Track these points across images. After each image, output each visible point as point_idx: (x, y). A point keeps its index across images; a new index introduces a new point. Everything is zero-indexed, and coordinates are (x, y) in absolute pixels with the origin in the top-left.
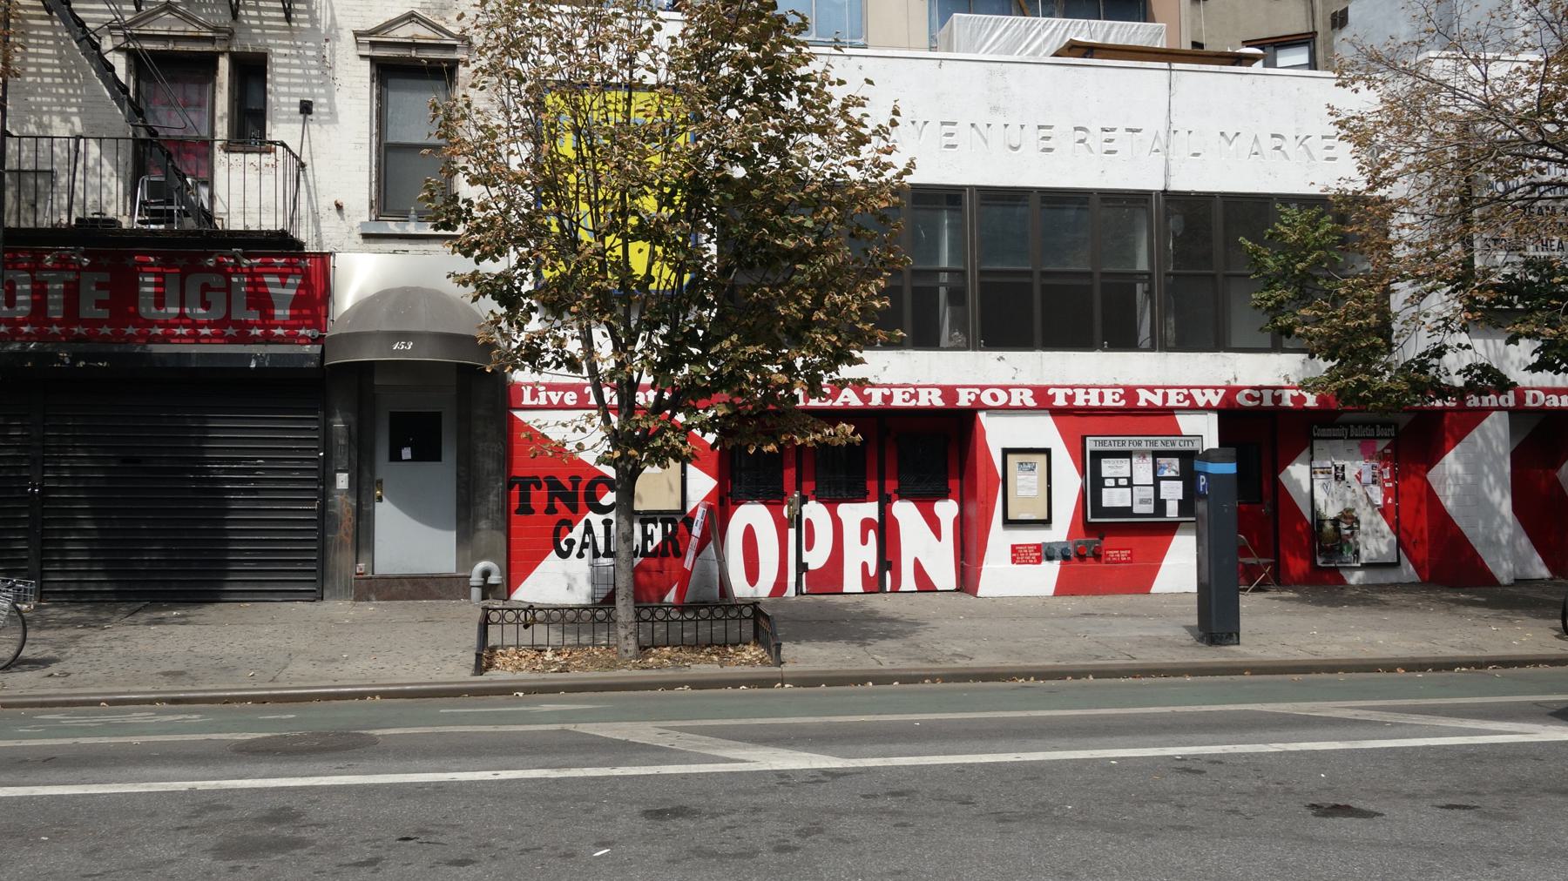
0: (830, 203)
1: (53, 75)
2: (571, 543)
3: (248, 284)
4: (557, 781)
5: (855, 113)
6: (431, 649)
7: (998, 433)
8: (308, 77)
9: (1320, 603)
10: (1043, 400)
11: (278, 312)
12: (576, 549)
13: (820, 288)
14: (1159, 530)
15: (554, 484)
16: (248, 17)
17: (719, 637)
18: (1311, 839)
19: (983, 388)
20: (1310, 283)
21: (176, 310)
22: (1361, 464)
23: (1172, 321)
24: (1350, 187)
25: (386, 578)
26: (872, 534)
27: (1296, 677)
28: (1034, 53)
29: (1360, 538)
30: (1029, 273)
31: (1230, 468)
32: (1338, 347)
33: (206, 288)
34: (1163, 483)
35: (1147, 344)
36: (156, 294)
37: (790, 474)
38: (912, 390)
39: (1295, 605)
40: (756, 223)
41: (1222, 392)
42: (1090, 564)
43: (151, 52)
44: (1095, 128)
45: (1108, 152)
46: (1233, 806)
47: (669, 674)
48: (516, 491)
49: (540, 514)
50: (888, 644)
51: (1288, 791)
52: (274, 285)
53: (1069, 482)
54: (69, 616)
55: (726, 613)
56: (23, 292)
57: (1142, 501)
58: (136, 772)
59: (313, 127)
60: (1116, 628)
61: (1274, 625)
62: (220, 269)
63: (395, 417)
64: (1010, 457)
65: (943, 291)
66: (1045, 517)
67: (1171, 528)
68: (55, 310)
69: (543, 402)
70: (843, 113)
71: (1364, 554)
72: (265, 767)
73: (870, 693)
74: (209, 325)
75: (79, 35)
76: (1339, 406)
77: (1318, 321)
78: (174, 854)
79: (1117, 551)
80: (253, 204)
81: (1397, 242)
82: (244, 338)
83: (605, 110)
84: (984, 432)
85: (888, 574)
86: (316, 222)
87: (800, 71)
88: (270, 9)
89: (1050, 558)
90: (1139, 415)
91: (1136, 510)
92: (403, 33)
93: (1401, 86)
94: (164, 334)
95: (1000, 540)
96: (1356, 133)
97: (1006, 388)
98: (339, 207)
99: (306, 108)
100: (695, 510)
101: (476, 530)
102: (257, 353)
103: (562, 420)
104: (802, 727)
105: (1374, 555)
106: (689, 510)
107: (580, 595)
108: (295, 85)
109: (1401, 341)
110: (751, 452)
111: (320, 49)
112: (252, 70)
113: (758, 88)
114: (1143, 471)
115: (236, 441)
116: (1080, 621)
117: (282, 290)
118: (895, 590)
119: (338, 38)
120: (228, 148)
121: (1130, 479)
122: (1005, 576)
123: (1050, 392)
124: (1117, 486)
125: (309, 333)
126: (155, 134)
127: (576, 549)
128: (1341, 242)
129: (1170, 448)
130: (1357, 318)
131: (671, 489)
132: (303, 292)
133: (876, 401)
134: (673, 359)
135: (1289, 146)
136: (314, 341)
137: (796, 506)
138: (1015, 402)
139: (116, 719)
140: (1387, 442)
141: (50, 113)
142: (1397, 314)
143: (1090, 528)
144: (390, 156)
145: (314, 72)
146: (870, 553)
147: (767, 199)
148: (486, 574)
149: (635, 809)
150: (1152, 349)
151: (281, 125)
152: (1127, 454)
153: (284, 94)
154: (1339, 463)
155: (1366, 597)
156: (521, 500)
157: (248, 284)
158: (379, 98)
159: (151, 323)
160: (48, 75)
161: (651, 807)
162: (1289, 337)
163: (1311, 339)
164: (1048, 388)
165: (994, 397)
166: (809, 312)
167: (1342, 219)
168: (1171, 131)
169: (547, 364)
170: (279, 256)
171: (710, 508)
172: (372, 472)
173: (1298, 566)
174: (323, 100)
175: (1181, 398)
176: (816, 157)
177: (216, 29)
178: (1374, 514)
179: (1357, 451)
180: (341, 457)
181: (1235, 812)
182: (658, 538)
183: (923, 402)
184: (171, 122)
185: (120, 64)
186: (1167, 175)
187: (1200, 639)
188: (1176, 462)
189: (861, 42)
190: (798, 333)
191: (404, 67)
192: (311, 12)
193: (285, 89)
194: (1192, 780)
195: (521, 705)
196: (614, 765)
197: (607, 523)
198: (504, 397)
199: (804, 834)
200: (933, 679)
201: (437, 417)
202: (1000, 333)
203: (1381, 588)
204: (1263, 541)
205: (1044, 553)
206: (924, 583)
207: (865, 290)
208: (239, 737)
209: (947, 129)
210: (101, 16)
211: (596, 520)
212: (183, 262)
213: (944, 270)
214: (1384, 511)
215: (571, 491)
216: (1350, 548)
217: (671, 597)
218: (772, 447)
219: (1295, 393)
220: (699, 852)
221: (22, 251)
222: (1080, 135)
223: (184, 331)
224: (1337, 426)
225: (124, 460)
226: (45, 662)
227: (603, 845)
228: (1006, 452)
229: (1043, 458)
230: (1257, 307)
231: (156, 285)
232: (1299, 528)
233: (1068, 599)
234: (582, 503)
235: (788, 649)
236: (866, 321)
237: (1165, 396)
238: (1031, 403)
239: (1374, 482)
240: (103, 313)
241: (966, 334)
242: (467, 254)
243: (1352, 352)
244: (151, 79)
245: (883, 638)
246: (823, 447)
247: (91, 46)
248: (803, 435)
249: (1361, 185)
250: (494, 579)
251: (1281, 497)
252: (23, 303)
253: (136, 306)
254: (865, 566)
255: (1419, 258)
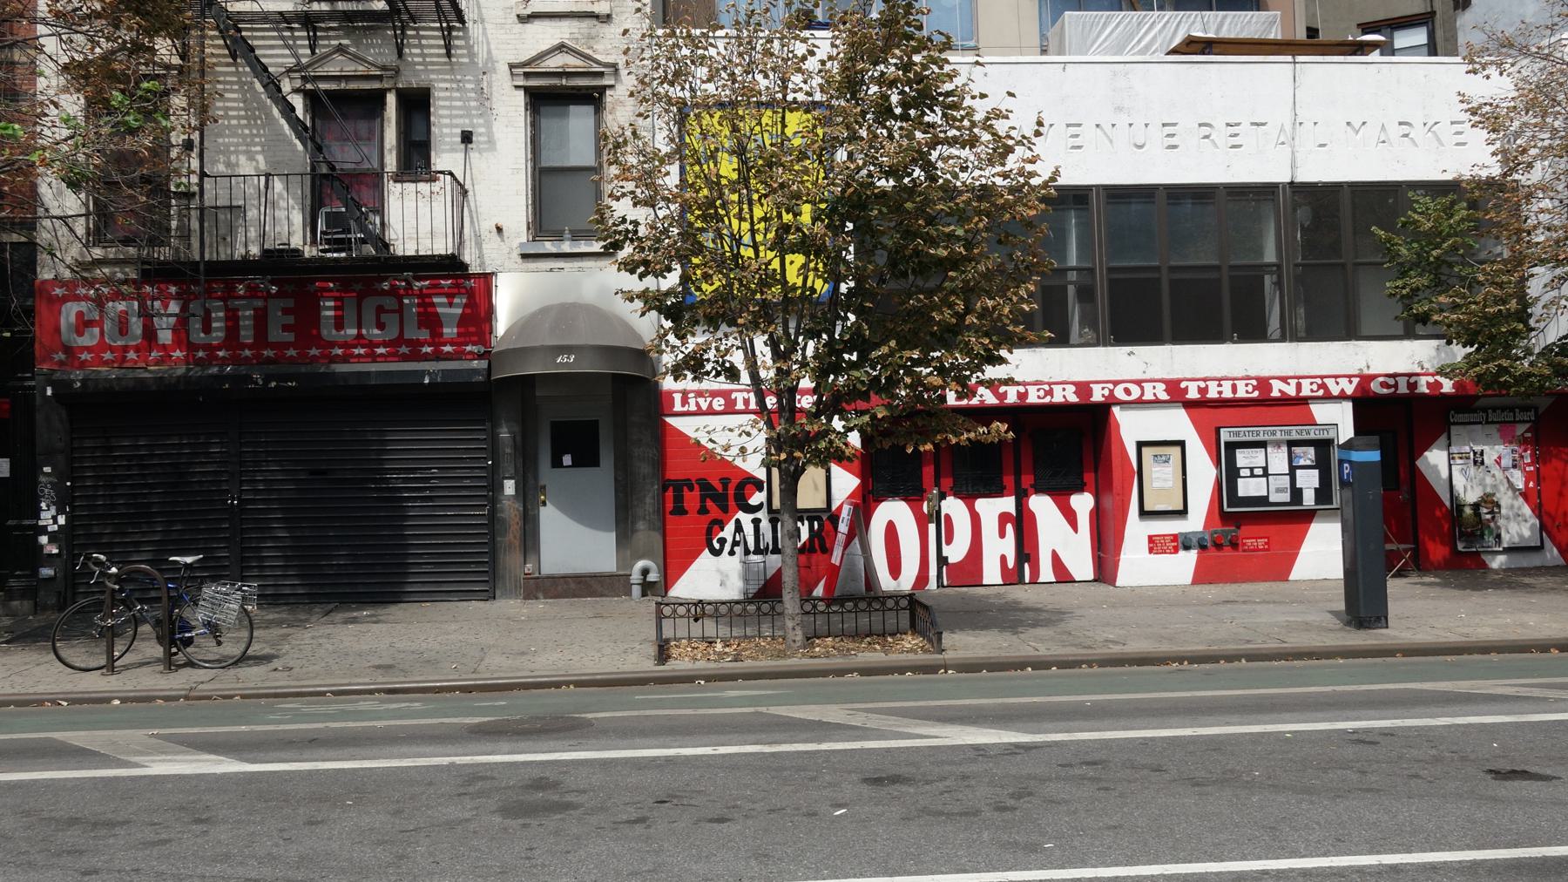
0: (979, 213)
1: (238, 118)
2: (722, 541)
3: (419, 305)
4: (773, 754)
5: (1001, 126)
6: (611, 642)
7: (1131, 427)
8: (467, 109)
9: (1463, 587)
10: (1176, 393)
11: (446, 330)
12: (727, 547)
13: (969, 292)
14: (1296, 518)
15: (705, 486)
16: (412, 55)
17: (877, 627)
18: (1495, 799)
19: (1116, 383)
20: (1444, 269)
21: (354, 332)
22: (1501, 449)
23: (1302, 311)
24: (1484, 174)
25: (552, 578)
26: (1009, 528)
27: (1449, 658)
28: (1147, 47)
29: (1501, 522)
30: (1157, 269)
31: (1374, 456)
32: (1477, 333)
33: (380, 310)
34: (1299, 472)
35: (1277, 334)
36: (336, 317)
37: (928, 471)
38: (1047, 387)
39: (1438, 589)
40: (909, 234)
41: (1356, 381)
42: (1228, 553)
43: (326, 91)
44: (1219, 123)
45: (1233, 147)
46: (1413, 771)
47: (838, 661)
48: (670, 493)
49: (693, 515)
50: (1040, 631)
51: (1464, 759)
52: (442, 305)
53: (1203, 473)
54: (271, 617)
55: (870, 605)
56: (218, 319)
57: (1278, 490)
58: (395, 750)
59: (473, 155)
60: (1250, 613)
61: (1421, 609)
62: (394, 291)
63: (555, 426)
64: (1145, 450)
65: (1071, 289)
66: (1181, 507)
67: (1308, 516)
68: (247, 336)
69: (693, 408)
70: (988, 128)
71: (1506, 537)
72: (505, 746)
73: (1029, 677)
74: (385, 344)
75: (266, 81)
76: (1480, 391)
77: (1455, 307)
78: (467, 815)
79: (1254, 539)
80: (424, 228)
81: (1535, 227)
82: (416, 356)
83: (762, 130)
84: (1118, 426)
85: (1026, 566)
86: (479, 245)
87: (948, 87)
88: (432, 46)
89: (1187, 548)
90: (1271, 406)
91: (1271, 499)
92: (555, 63)
93: (1530, 69)
94: (345, 354)
95: (1136, 531)
96: (1489, 118)
97: (1139, 383)
98: (499, 230)
99: (467, 138)
100: (840, 508)
101: (634, 531)
102: (430, 370)
103: (723, 429)
104: (980, 708)
105: (1516, 540)
106: (834, 508)
107: (733, 589)
108: (456, 116)
109: (1542, 324)
110: (909, 451)
111: (479, 82)
112: (417, 104)
113: (905, 105)
114: (1278, 461)
115: (415, 454)
116: (1223, 608)
117: (450, 310)
118: (1034, 581)
119: (494, 70)
120: (398, 178)
121: (1265, 469)
122: (1139, 565)
123: (1183, 385)
124: (1252, 475)
125: (475, 349)
126: (333, 168)
127: (727, 547)
128: (1476, 228)
129: (1305, 437)
130: (1496, 304)
131: (816, 488)
132: (468, 311)
133: (1012, 398)
134: (827, 366)
135: (1417, 133)
136: (480, 356)
137: (935, 501)
138: (1148, 396)
139: (349, 707)
140: (1527, 425)
141: (237, 152)
142: (1537, 299)
143: (1226, 518)
144: (546, 181)
145: (473, 104)
146: (1008, 546)
147: (920, 211)
148: (645, 572)
149: (854, 777)
150: (1282, 339)
151: (444, 155)
152: (1262, 445)
153: (446, 126)
154: (1478, 448)
155: (1509, 581)
156: (677, 501)
157: (419, 305)
158: (533, 125)
159: (332, 345)
160: (234, 117)
161: (867, 775)
162: (1425, 324)
163: (1449, 326)
164: (1180, 381)
165: (1127, 391)
166: (961, 317)
167: (1473, 205)
168: (1297, 123)
169: (708, 373)
170: (446, 278)
171: (856, 506)
172: (536, 478)
173: (1438, 551)
174: (482, 130)
175: (1315, 387)
176: (966, 168)
177: (384, 68)
178: (1515, 498)
179: (1496, 435)
180: (508, 466)
181: (1417, 776)
182: (805, 534)
183: (1058, 398)
184: (346, 156)
185: (298, 102)
186: (1293, 167)
187: (1348, 623)
188: (1311, 450)
189: (972, 44)
190: (949, 337)
191: (553, 95)
192: (469, 47)
193: (447, 121)
194: (1369, 750)
195: (702, 691)
196: (820, 741)
197: (756, 522)
198: (658, 404)
199: (1017, 796)
200: (1090, 664)
201: (594, 425)
202: (1131, 326)
203: (1525, 571)
204: (1409, 531)
205: (1181, 543)
206: (1063, 575)
207: (1016, 294)
208: (468, 720)
209: (1073, 130)
210: (280, 60)
211: (746, 519)
212: (358, 287)
213: (1072, 269)
214: (1525, 495)
215: (729, 490)
216: (1491, 533)
217: (819, 591)
218: (929, 447)
219: (1431, 379)
220: (925, 811)
221: (216, 281)
222: (1205, 130)
223: (362, 351)
224: (1475, 411)
225: (312, 473)
226: (267, 658)
227: (840, 806)
228: (1140, 445)
229: (1177, 450)
230: (1391, 295)
231: (336, 308)
232: (1438, 513)
233: (1207, 587)
234: (732, 503)
235: (948, 639)
236: (1016, 323)
237: (1299, 387)
238: (1164, 396)
239: (1514, 466)
240: (289, 337)
241: (1096, 330)
242: (632, 272)
243: (1492, 337)
244: (327, 117)
245: (1034, 626)
246: (975, 444)
247: (272, 86)
248: (956, 434)
249: (1496, 171)
250: (652, 577)
251: (1418, 484)
252: (218, 329)
253: (318, 329)
254: (1003, 559)
255: (1557, 242)
